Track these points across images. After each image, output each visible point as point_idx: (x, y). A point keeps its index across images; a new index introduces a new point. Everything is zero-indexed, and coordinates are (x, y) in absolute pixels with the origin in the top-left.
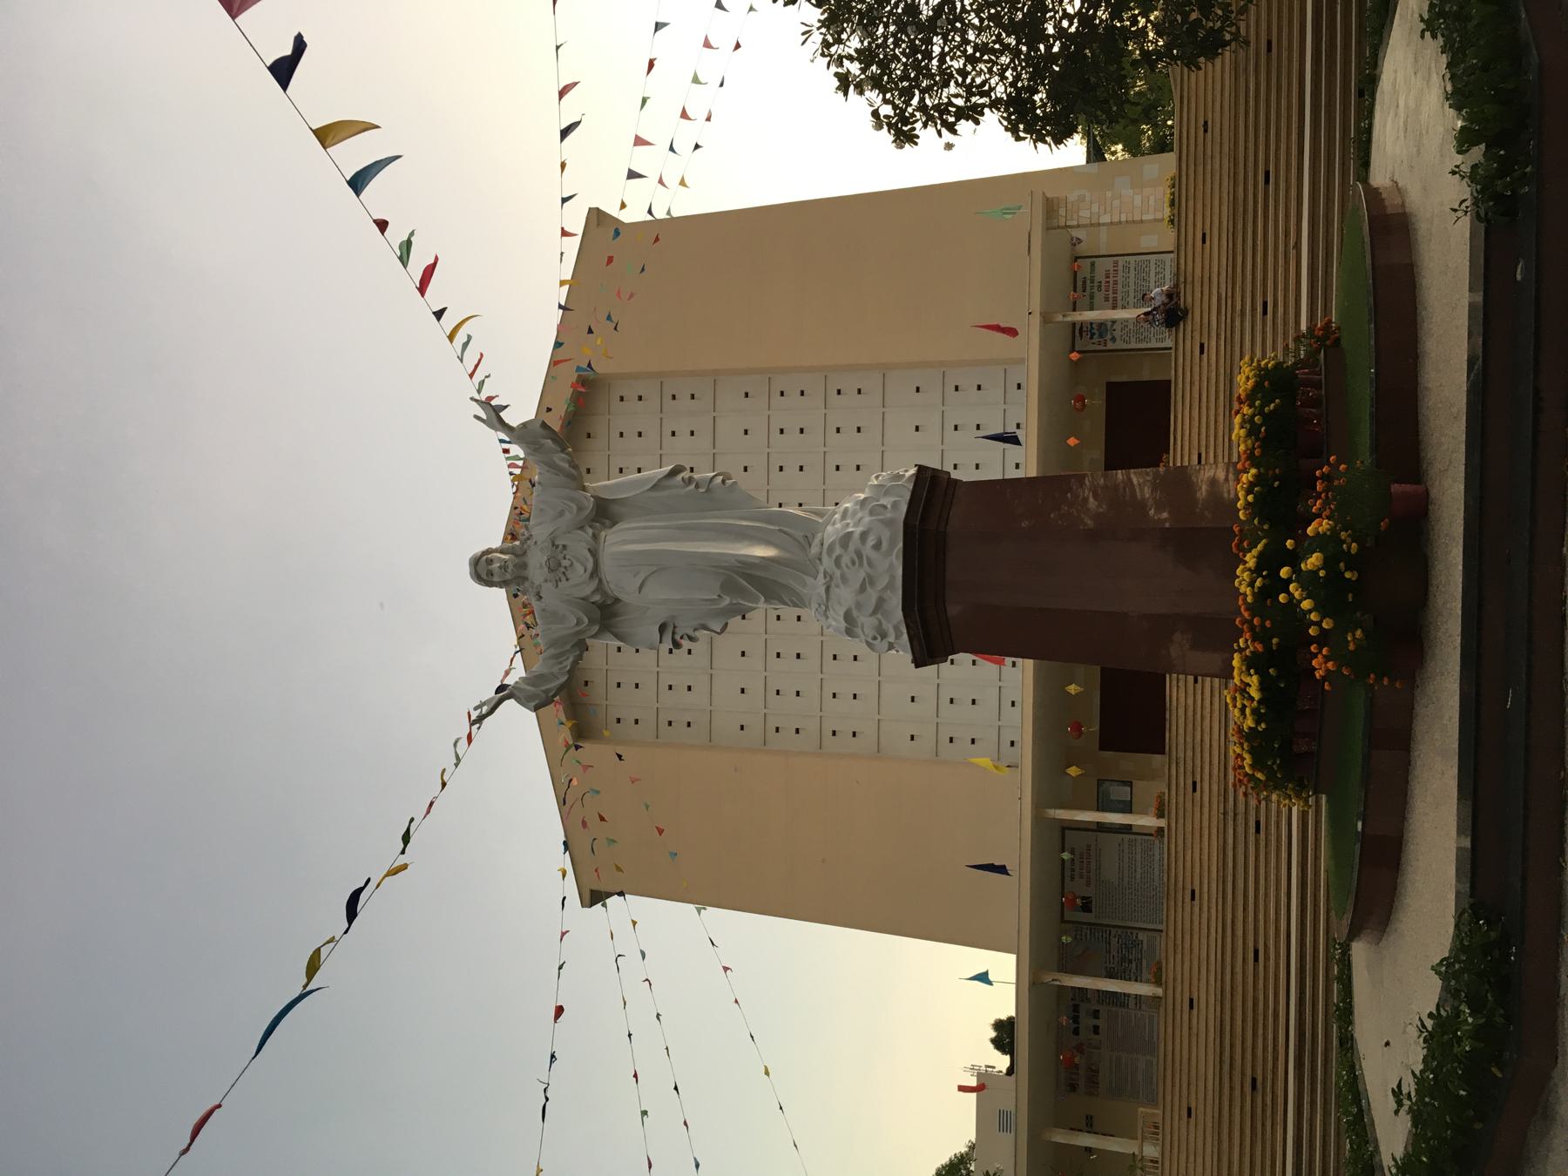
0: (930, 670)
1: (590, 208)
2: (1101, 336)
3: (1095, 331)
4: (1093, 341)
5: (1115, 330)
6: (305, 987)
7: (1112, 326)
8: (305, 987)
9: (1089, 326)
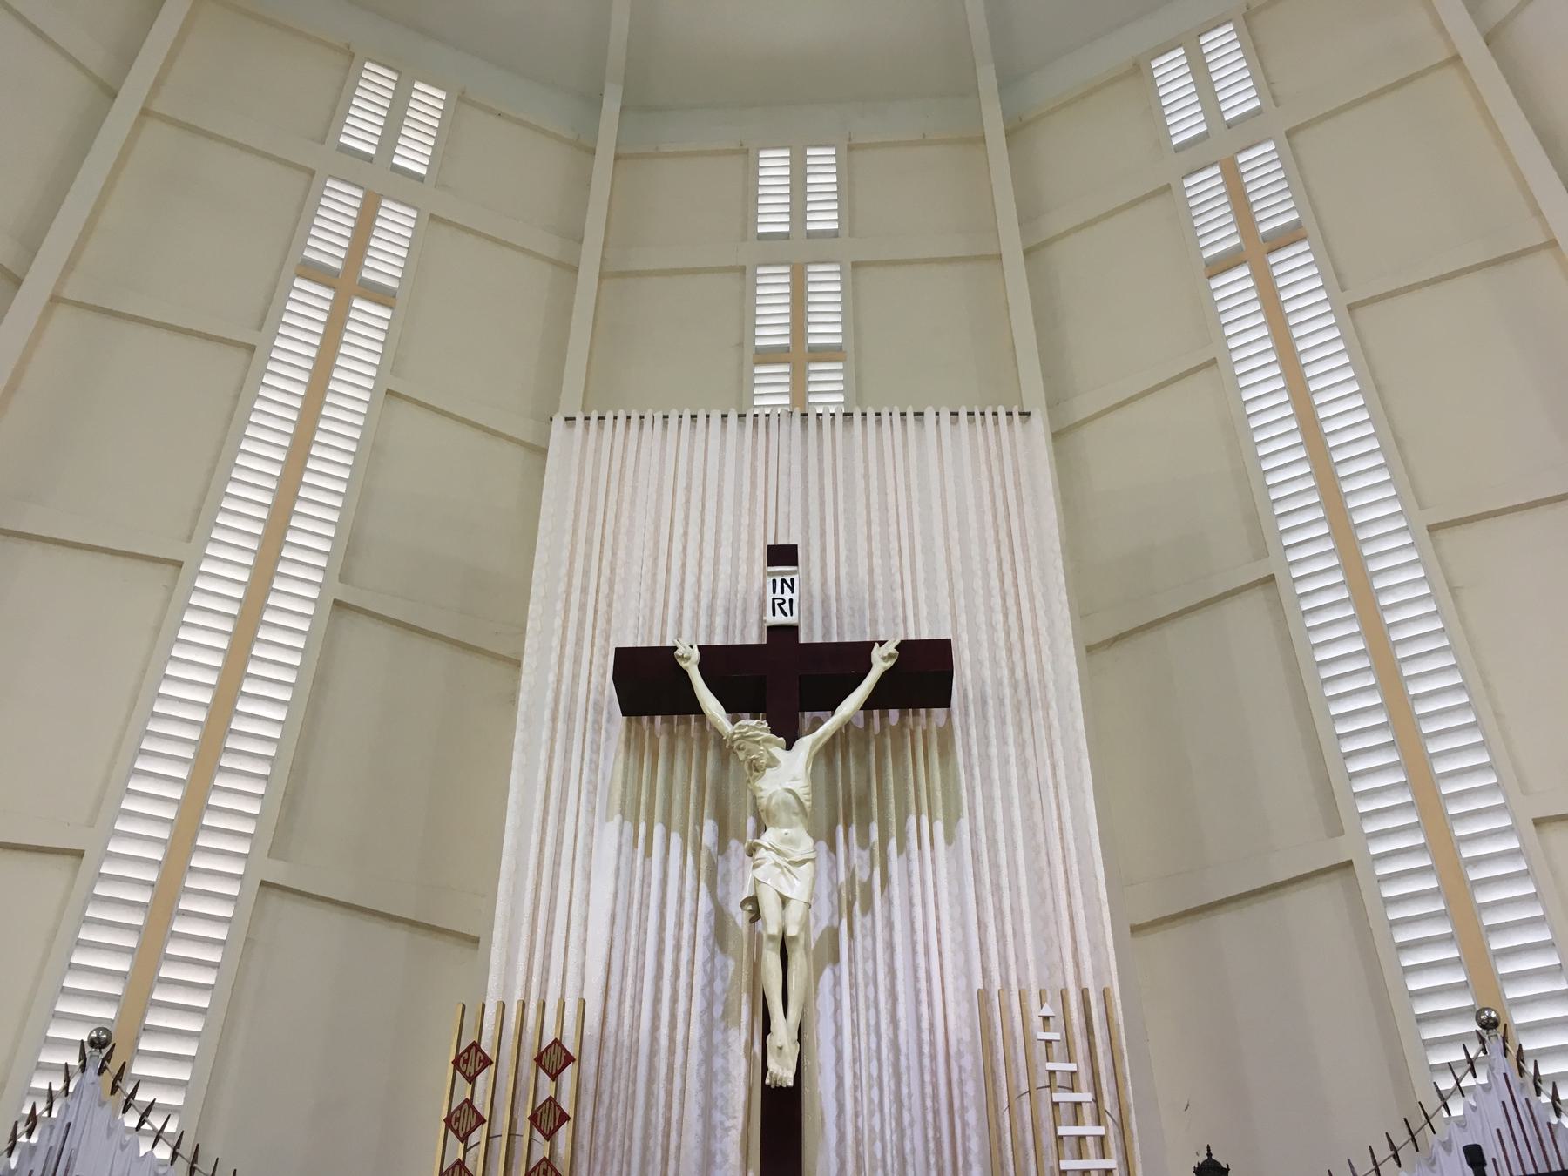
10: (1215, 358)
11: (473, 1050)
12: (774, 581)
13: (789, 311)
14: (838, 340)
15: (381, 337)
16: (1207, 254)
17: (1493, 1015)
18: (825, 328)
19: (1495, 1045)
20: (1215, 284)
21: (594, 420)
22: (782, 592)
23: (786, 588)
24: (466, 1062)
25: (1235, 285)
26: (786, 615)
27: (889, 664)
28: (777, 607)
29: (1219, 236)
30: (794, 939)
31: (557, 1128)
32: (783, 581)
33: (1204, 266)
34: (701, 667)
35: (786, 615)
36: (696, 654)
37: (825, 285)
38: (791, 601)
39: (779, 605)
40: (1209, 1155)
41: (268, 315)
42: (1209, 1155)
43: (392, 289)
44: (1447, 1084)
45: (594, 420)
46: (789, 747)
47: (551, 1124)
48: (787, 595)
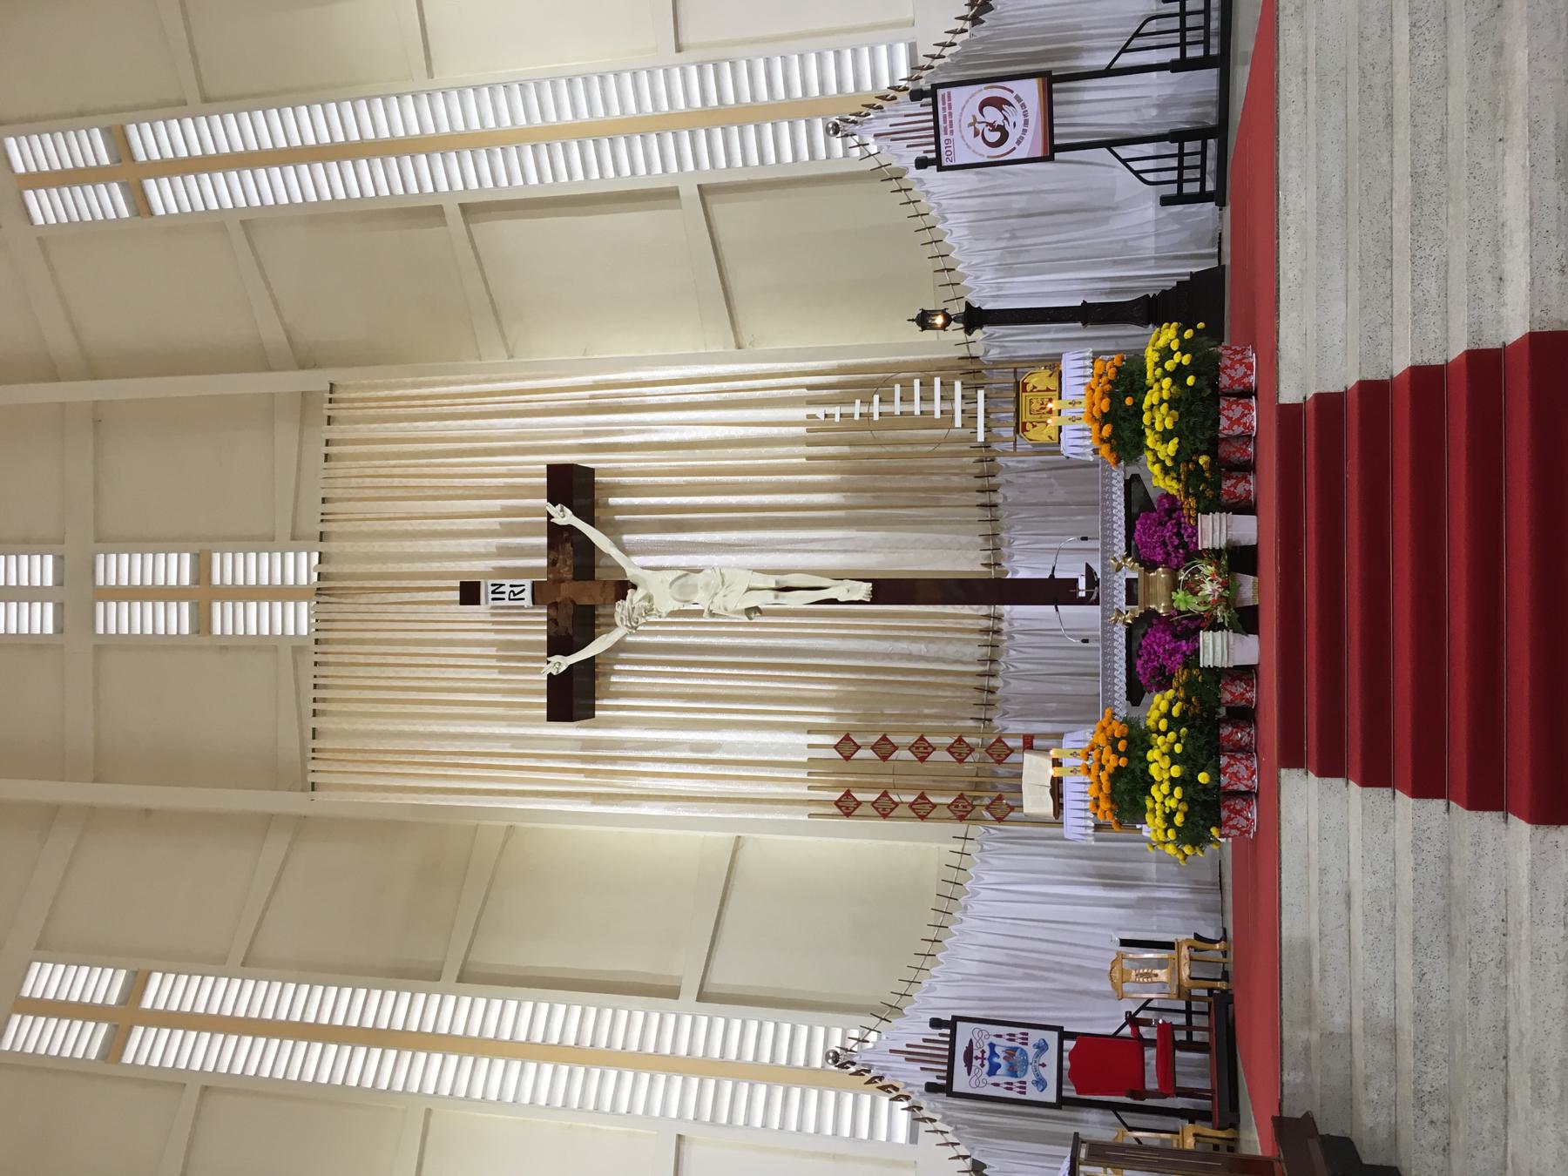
0: (1048, 783)
1: (224, 964)
2: (1013, 1072)
3: (1000, 1061)
4: (994, 1079)
5: (1044, 1065)
6: (686, 575)
7: (1037, 1056)
8: (686, 575)
9: (987, 1049)
10: (241, 221)
11: (840, 804)
12: (493, 599)
13: (139, 603)
14: (187, 557)
15: (66, 1053)
16: (125, 213)
17: (830, 126)
18: (175, 568)
19: (851, 128)
20: (159, 210)
21: (314, 755)
22: (504, 593)
23: (501, 590)
24: (847, 808)
25: (163, 196)
26: (523, 590)
27: (568, 511)
28: (517, 597)
29: (110, 201)
30: (777, 582)
31: (891, 743)
32: (493, 592)
33: (139, 218)
34: (567, 653)
35: (523, 590)
36: (556, 659)
37: (117, 568)
38: (511, 586)
39: (515, 595)
40: (913, 320)
41: (170, 1081)
42: (913, 320)
43: (127, 977)
44: (856, 152)
45: (314, 755)
46: (635, 587)
47: (888, 746)
48: (507, 589)
